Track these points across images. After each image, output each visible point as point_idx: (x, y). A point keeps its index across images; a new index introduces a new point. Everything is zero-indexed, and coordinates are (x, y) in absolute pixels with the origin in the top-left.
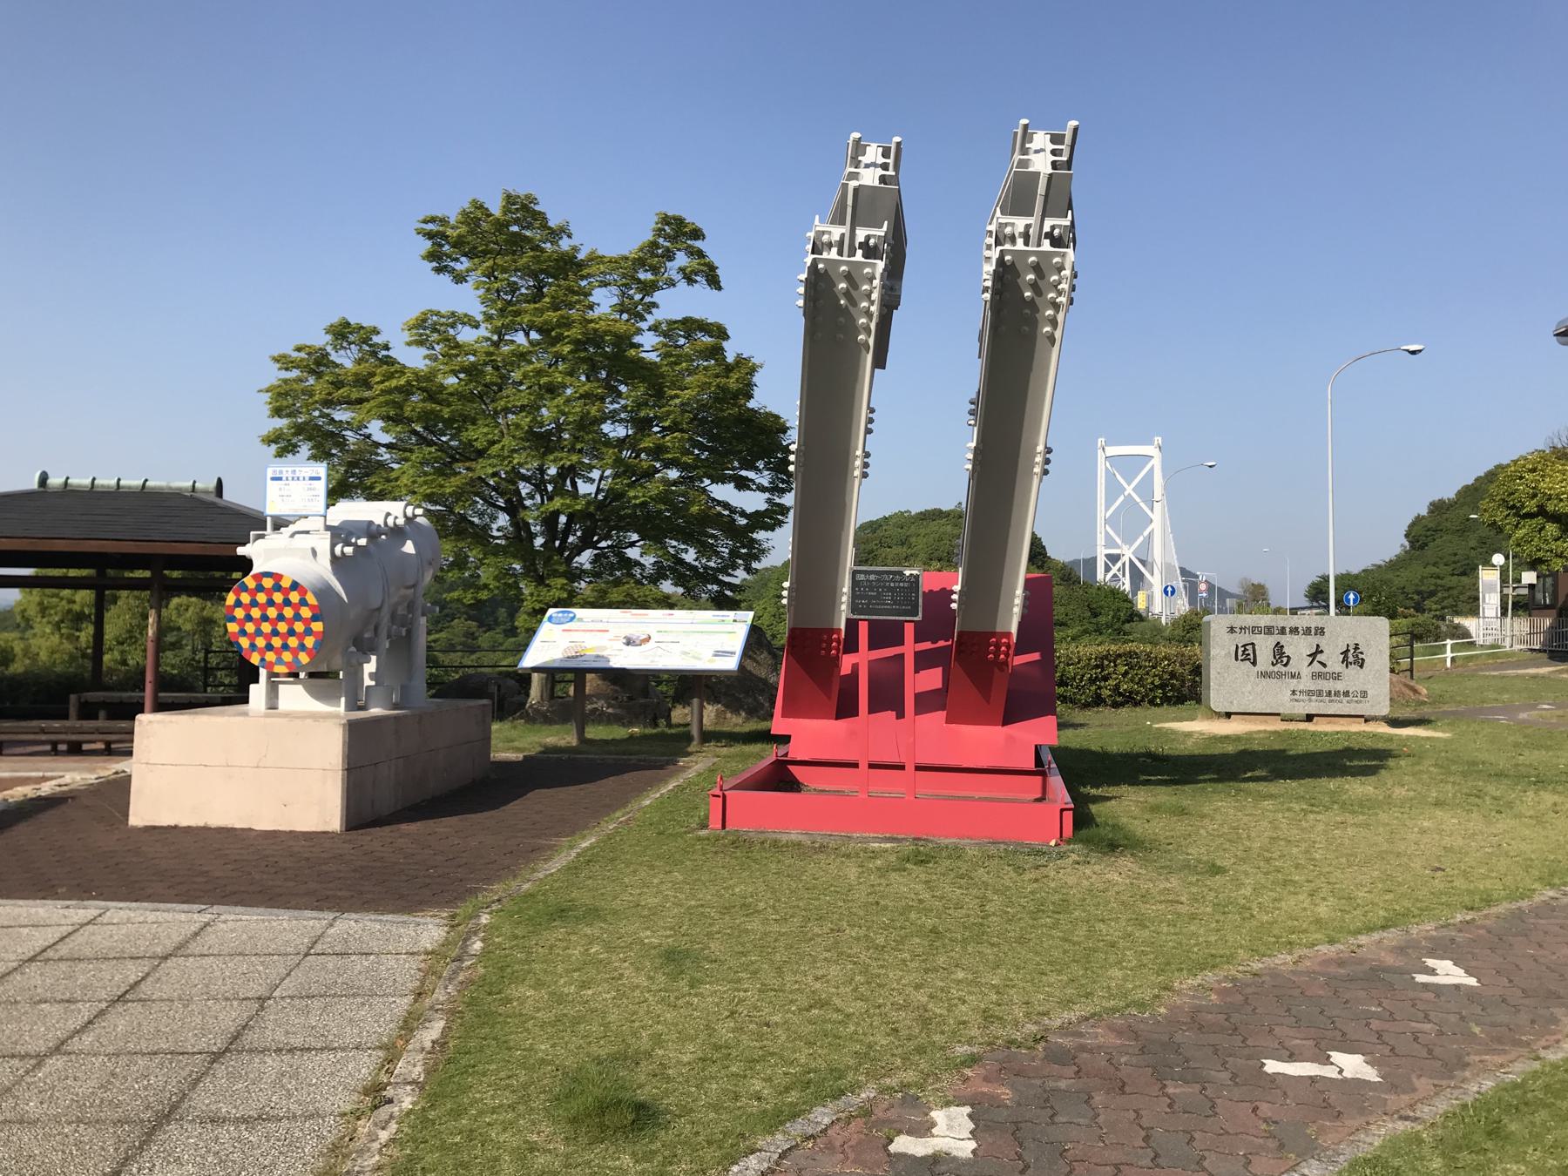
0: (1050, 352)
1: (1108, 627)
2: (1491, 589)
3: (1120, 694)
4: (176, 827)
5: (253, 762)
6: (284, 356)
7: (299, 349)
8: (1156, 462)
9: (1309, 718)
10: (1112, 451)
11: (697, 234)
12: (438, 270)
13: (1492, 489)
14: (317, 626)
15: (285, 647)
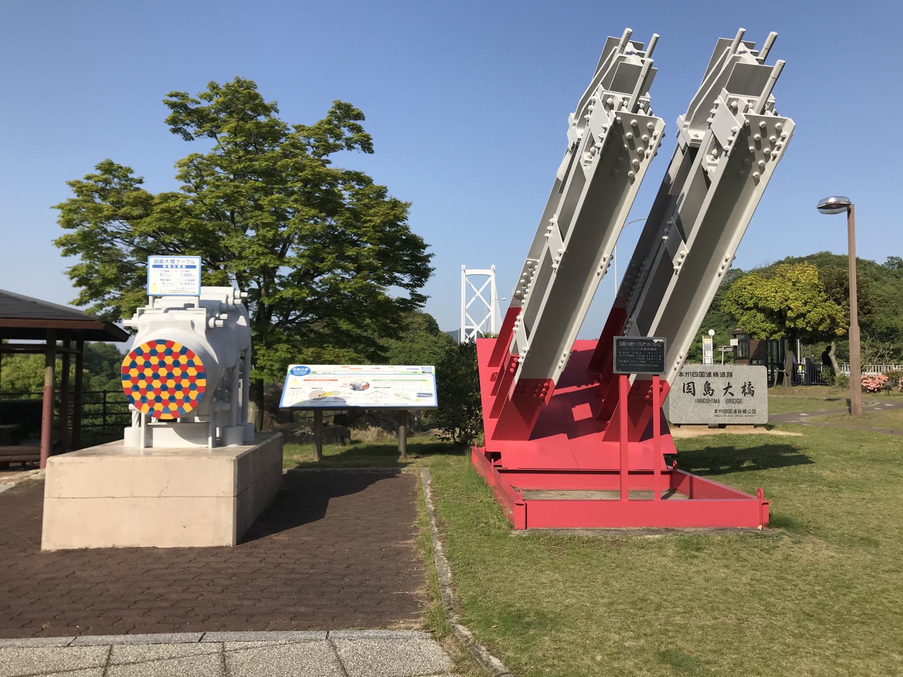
0: (753, 189)
4: (86, 550)
5: (146, 490)
6: (79, 182)
7: (88, 178)
8: (492, 279)
9: (722, 426)
11: (359, 116)
12: (174, 131)
13: (729, 293)
14: (202, 383)
15: (172, 399)
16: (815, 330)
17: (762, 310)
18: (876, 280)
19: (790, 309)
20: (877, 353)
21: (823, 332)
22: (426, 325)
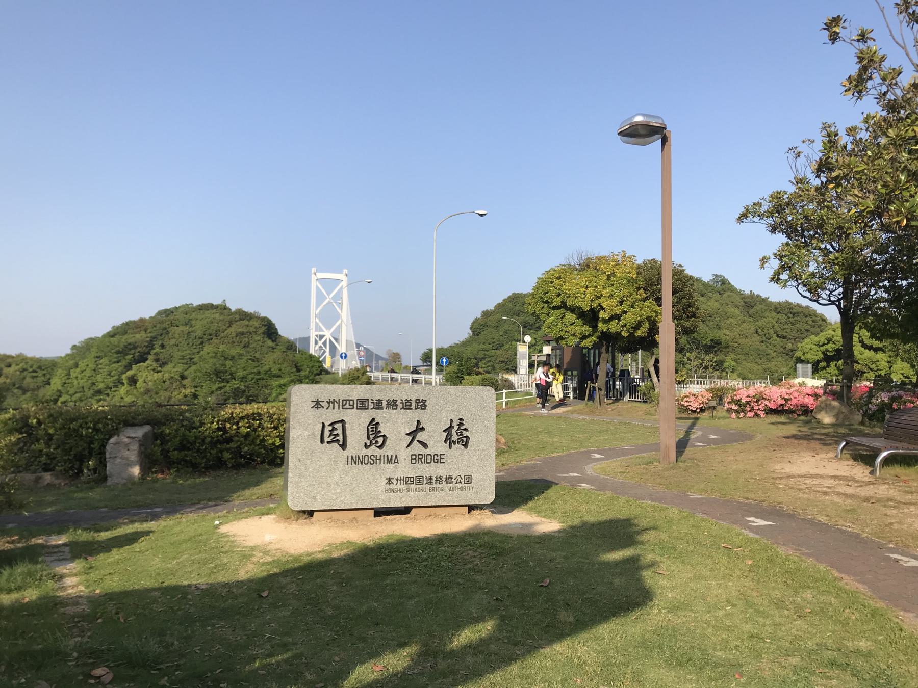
2: (524, 358)
3: (242, 456)
8: (344, 284)
10: (321, 275)
16: (632, 335)
17: (572, 310)
18: (702, 295)
19: (603, 309)
20: (701, 364)
21: (641, 338)
22: (263, 329)
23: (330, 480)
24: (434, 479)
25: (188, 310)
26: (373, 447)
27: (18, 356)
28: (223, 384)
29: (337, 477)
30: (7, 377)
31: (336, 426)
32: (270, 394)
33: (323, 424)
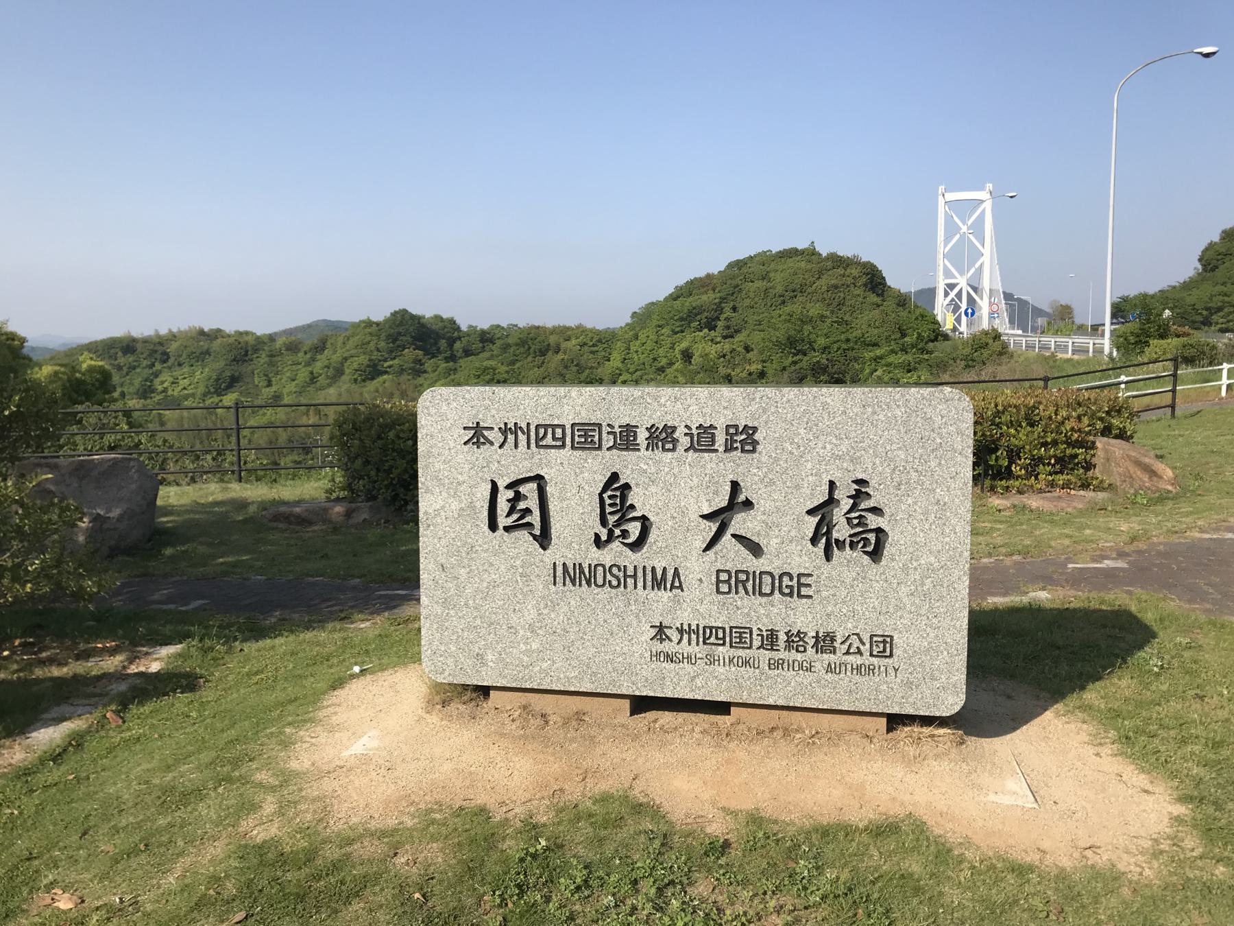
1: (913, 347)
2: (28, 749)
8: (988, 206)
10: (951, 196)
23: (514, 620)
24: (782, 637)
25: (765, 259)
26: (616, 545)
27: (578, 327)
28: (798, 357)
29: (530, 614)
30: (565, 353)
31: (523, 489)
32: (862, 370)
33: (494, 484)
